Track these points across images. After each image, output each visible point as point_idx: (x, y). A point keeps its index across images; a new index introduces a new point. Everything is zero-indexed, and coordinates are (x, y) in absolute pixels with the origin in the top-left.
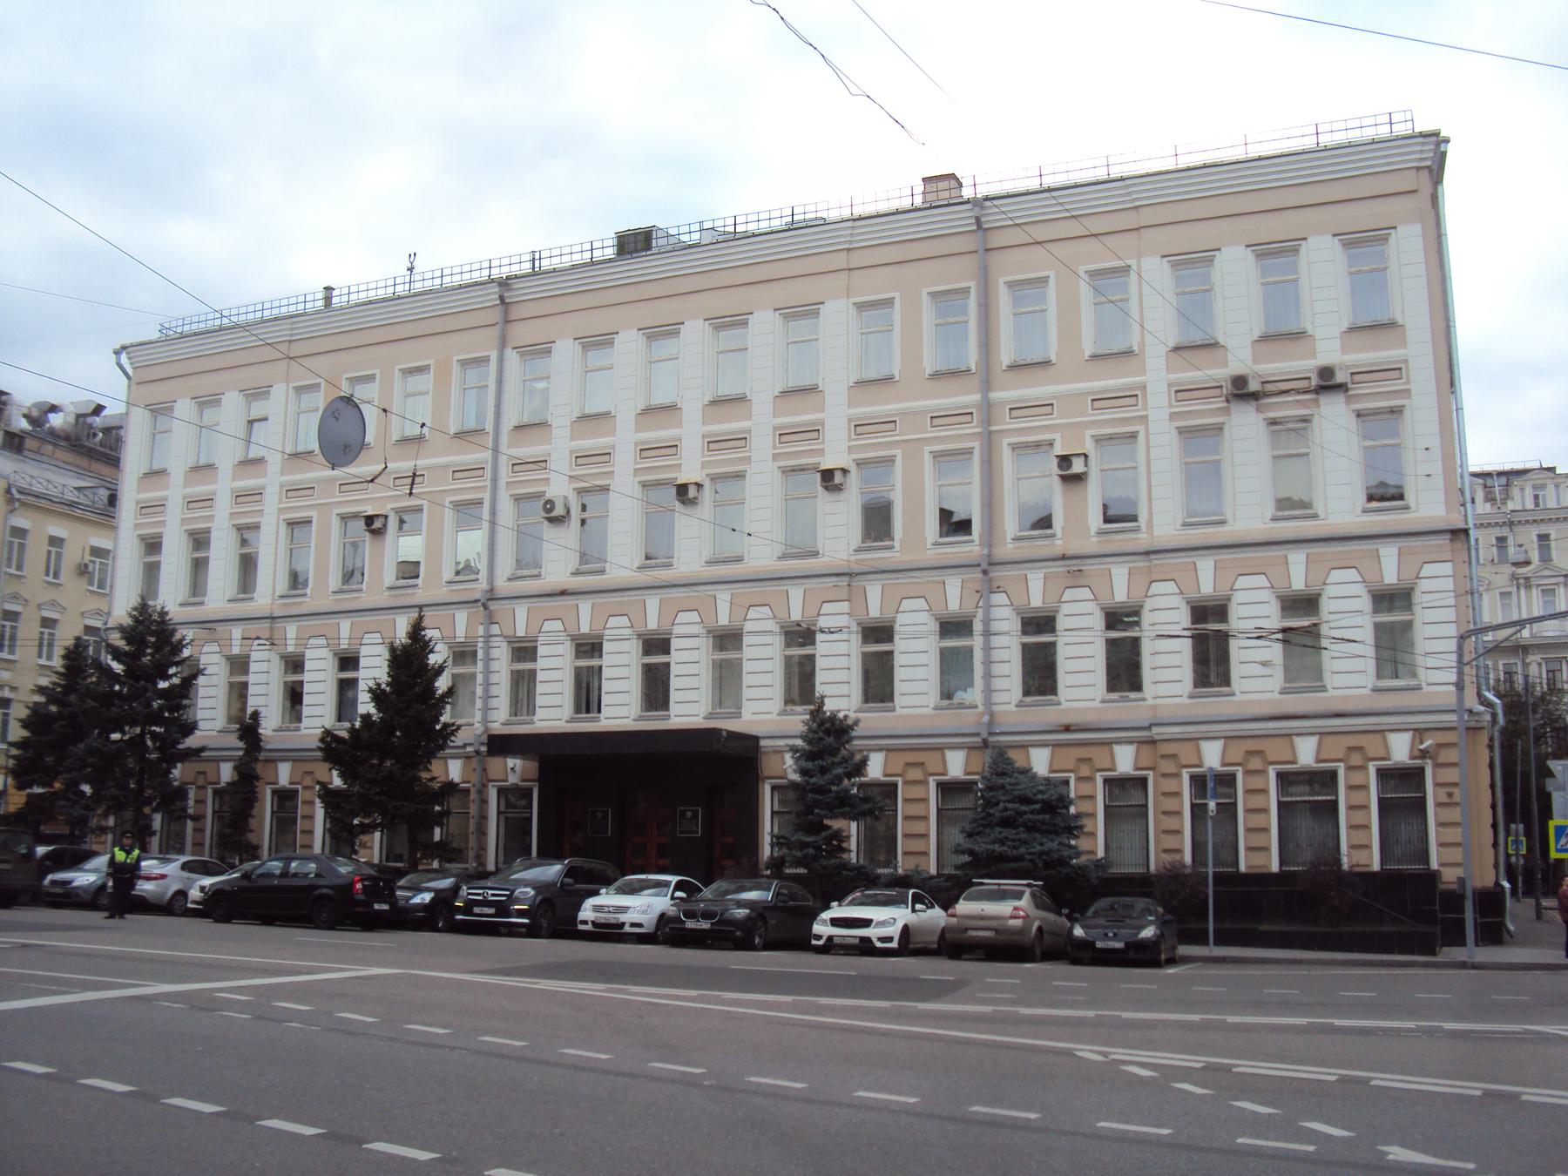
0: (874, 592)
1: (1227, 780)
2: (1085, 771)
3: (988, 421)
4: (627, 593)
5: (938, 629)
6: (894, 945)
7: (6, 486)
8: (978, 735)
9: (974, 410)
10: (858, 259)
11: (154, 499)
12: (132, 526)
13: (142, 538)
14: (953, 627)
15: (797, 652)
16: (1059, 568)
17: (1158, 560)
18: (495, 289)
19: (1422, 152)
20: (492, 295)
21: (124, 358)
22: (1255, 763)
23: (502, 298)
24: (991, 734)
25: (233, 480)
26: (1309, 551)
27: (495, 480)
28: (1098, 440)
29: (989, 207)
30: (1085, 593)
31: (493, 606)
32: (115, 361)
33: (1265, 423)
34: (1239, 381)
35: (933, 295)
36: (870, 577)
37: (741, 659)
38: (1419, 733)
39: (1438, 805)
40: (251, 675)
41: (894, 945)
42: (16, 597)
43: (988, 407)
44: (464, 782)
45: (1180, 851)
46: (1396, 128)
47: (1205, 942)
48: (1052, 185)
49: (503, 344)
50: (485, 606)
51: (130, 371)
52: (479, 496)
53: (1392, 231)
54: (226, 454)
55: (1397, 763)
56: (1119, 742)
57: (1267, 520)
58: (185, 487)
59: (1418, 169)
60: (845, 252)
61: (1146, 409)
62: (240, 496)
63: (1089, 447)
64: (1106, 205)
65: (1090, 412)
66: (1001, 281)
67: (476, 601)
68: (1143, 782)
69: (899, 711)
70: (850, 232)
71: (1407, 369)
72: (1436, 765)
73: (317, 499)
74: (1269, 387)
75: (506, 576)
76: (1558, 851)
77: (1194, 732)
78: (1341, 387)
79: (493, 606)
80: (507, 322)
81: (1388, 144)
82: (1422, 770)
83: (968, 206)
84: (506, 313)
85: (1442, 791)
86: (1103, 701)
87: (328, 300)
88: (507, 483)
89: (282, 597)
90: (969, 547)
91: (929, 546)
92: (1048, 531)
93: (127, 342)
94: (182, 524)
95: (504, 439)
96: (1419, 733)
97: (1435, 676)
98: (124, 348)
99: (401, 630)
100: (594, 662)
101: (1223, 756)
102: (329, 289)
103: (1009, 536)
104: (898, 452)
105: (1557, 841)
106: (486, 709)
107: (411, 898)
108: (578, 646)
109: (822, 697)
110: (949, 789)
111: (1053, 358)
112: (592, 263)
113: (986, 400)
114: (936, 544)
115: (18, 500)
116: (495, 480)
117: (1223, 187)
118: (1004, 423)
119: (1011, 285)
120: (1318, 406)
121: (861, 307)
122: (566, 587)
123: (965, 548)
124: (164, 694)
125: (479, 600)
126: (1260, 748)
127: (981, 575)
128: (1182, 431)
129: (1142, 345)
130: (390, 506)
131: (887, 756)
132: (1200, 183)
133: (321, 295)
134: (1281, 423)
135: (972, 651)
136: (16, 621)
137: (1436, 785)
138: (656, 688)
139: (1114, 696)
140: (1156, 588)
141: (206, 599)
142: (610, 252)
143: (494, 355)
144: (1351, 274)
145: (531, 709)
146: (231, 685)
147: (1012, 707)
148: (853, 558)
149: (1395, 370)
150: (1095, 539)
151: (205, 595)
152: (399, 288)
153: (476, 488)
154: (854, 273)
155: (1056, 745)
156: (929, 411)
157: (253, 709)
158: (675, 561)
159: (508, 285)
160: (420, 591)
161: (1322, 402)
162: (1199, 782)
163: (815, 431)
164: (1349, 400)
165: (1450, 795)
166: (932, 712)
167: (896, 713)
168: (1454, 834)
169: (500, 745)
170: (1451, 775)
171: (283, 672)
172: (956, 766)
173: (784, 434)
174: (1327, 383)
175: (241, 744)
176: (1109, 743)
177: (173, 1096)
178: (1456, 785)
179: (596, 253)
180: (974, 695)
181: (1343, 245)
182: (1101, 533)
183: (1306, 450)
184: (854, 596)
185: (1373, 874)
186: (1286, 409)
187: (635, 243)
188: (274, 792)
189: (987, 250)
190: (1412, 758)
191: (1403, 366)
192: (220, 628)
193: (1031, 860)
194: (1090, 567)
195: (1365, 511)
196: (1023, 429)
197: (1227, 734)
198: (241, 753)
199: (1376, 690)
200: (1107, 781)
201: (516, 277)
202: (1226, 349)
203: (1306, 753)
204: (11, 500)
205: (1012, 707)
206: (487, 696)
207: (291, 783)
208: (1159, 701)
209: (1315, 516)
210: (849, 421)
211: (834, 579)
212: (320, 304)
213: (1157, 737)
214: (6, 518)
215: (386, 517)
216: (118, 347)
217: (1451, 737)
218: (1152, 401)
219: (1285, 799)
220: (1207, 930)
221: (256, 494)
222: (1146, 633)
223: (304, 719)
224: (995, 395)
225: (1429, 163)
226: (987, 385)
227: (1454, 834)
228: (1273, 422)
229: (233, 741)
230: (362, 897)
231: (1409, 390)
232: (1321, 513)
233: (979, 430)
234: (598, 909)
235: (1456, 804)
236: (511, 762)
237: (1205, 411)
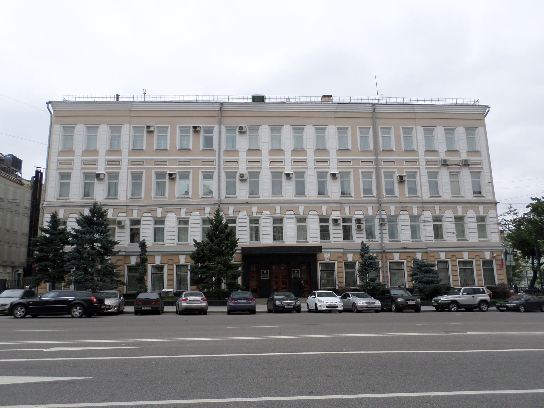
2: (171, 262)
4: (269, 204)
12: (56, 169)
15: (182, 226)
16: (399, 205)
17: (425, 205)
18: (219, 105)
20: (217, 107)
21: (50, 105)
22: (454, 258)
25: (106, 156)
26: (440, 205)
27: (219, 166)
29: (377, 106)
30: (406, 212)
32: (46, 107)
36: (346, 204)
43: (377, 162)
46: (154, 99)
48: (317, 102)
51: (52, 113)
58: (82, 156)
59: (216, 111)
60: (334, 113)
61: (97, 166)
65: (201, 165)
68: (471, 262)
71: (482, 162)
81: (409, 106)
82: (492, 261)
86: (177, 244)
87: (118, 98)
91: (152, 198)
95: (222, 153)
96: (492, 252)
97: (493, 238)
98: (50, 102)
99: (208, 213)
101: (353, 259)
102: (118, 95)
103: (176, 197)
104: (352, 170)
108: (274, 220)
113: (377, 158)
114: (130, 198)
116: (219, 166)
117: (423, 111)
121: (338, 128)
129: (418, 149)
130: (177, 171)
131: (353, 255)
132: (301, 107)
135: (236, 228)
138: (278, 233)
140: (425, 212)
142: (250, 100)
144: (425, 137)
146: (251, 228)
153: (208, 168)
155: (400, 253)
156: (405, 160)
157: (143, 238)
161: (463, 168)
163: (282, 162)
166: (176, 245)
173: (85, 162)
176: (415, 252)
181: (293, 128)
184: (342, 209)
186: (454, 169)
187: (259, 99)
189: (221, 116)
191: (72, 161)
195: (341, 196)
197: (446, 251)
200: (177, 266)
202: (284, 151)
203: (466, 256)
208: (403, 241)
209: (305, 197)
210: (337, 160)
211: (336, 204)
212: (115, 99)
216: (48, 101)
218: (421, 164)
222: (454, 223)
224: (374, 157)
231: (483, 168)
232: (307, 196)
237: (434, 168)
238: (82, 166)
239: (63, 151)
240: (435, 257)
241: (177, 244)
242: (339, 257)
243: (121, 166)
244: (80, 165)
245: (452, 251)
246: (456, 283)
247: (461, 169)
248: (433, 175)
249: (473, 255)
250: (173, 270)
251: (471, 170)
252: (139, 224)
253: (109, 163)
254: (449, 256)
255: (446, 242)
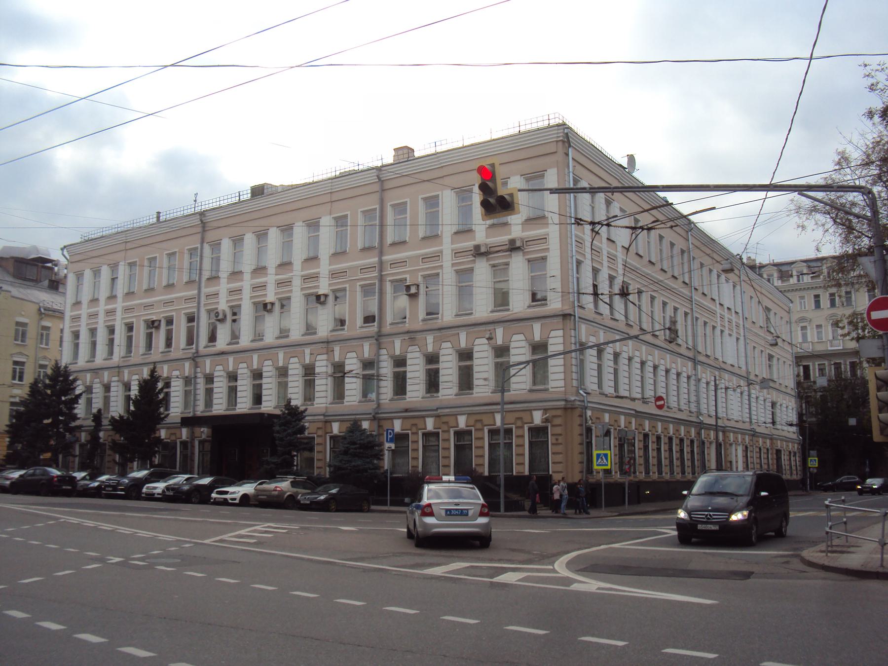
0: (337, 350)
1: (509, 432)
2: (479, 426)
3: (381, 271)
5: (362, 366)
6: (237, 501)
7: (38, 307)
8: (370, 414)
9: (376, 265)
10: (129, 246)
11: (129, 306)
12: (451, 265)
13: (126, 324)
14: (368, 364)
16: (406, 337)
19: (558, 133)
20: (196, 221)
23: (201, 221)
24: (376, 413)
28: (424, 277)
31: (198, 360)
33: (490, 267)
34: (477, 247)
35: (425, 199)
36: (334, 343)
37: (472, 365)
38: (546, 410)
39: (553, 444)
40: (408, 367)
41: (237, 501)
42: (45, 358)
43: (381, 263)
44: (166, 439)
45: (417, 467)
46: (196, 209)
47: (386, 505)
49: (202, 242)
50: (193, 360)
51: (68, 258)
52: (404, 276)
53: (545, 172)
54: (103, 294)
55: (536, 425)
56: (429, 416)
57: (489, 312)
58: (330, 265)
59: (557, 141)
62: (231, 292)
63: (420, 280)
64: (317, 193)
65: (389, 269)
66: (389, 204)
67: (190, 358)
69: (346, 404)
70: (330, 185)
72: (553, 426)
73: (408, 267)
74: (492, 249)
75: (203, 346)
76: (597, 465)
77: (455, 410)
78: (518, 248)
79: (198, 360)
80: (383, 190)
81: (544, 130)
82: (547, 428)
83: (375, 171)
84: (382, 185)
85: (554, 438)
87: (158, 217)
88: (204, 304)
89: (123, 357)
90: (373, 328)
91: (358, 328)
92: (507, 307)
93: (66, 244)
94: (275, 295)
95: (203, 284)
96: (546, 410)
98: (65, 247)
99: (146, 373)
100: (468, 363)
101: (434, 425)
102: (159, 213)
103: (358, 326)
104: (347, 286)
105: (597, 460)
106: (195, 406)
107: (89, 484)
109: (290, 399)
110: (334, 438)
111: (407, 239)
112: (240, 202)
115: (44, 314)
118: (388, 271)
119: (392, 206)
120: (475, 263)
122: (225, 350)
123: (371, 329)
124: (65, 402)
125: (374, 337)
126: (520, 416)
127: (375, 341)
128: (457, 272)
133: (155, 216)
134: (497, 266)
136: (46, 369)
137: (552, 435)
139: (428, 395)
141: (96, 359)
143: (199, 245)
145: (211, 406)
147: (387, 401)
148: (329, 335)
149: (544, 239)
150: (421, 323)
151: (216, 341)
152: (222, 202)
154: (334, 204)
155: (404, 418)
158: (474, 312)
159: (204, 214)
160: (132, 358)
161: (513, 255)
162: (493, 433)
164: (524, 254)
165: (557, 440)
167: (344, 404)
168: (559, 458)
169: (186, 422)
170: (558, 430)
171: (531, 354)
172: (336, 428)
174: (513, 247)
175: (93, 424)
177: (445, 615)
178: (560, 435)
179: (241, 197)
180: (373, 396)
182: (424, 320)
183: (507, 278)
185: (525, 476)
188: (331, 437)
190: (542, 422)
191: (547, 237)
192: (100, 372)
193: (351, 469)
194: (419, 336)
196: (395, 273)
198: (92, 428)
199: (531, 391)
201: (207, 211)
204: (41, 314)
205: (387, 401)
206: (195, 400)
207: (467, 426)
208: (444, 397)
211: (322, 344)
212: (155, 220)
213: (440, 414)
214: (39, 323)
215: (160, 321)
216: (62, 246)
217: (559, 412)
219: (493, 442)
220: (387, 500)
221: (288, 282)
223: (263, 403)
224: (384, 258)
225: (561, 138)
226: (381, 253)
227: (559, 458)
228: (494, 266)
229: (90, 423)
230: (57, 484)
233: (377, 274)
234: (148, 488)
235: (561, 444)
236: (202, 430)
238: (452, 260)
239: (335, 255)
240: (176, 436)
241: (422, 398)
242: (318, 428)
243: (442, 262)
244: (450, 259)
245: (412, 415)
246: (520, 468)
247: (510, 256)
248: (464, 274)
249: (510, 418)
250: (483, 438)
251: (492, 262)
252: (437, 362)
253: (457, 255)
254: (472, 422)
255: (474, 396)
